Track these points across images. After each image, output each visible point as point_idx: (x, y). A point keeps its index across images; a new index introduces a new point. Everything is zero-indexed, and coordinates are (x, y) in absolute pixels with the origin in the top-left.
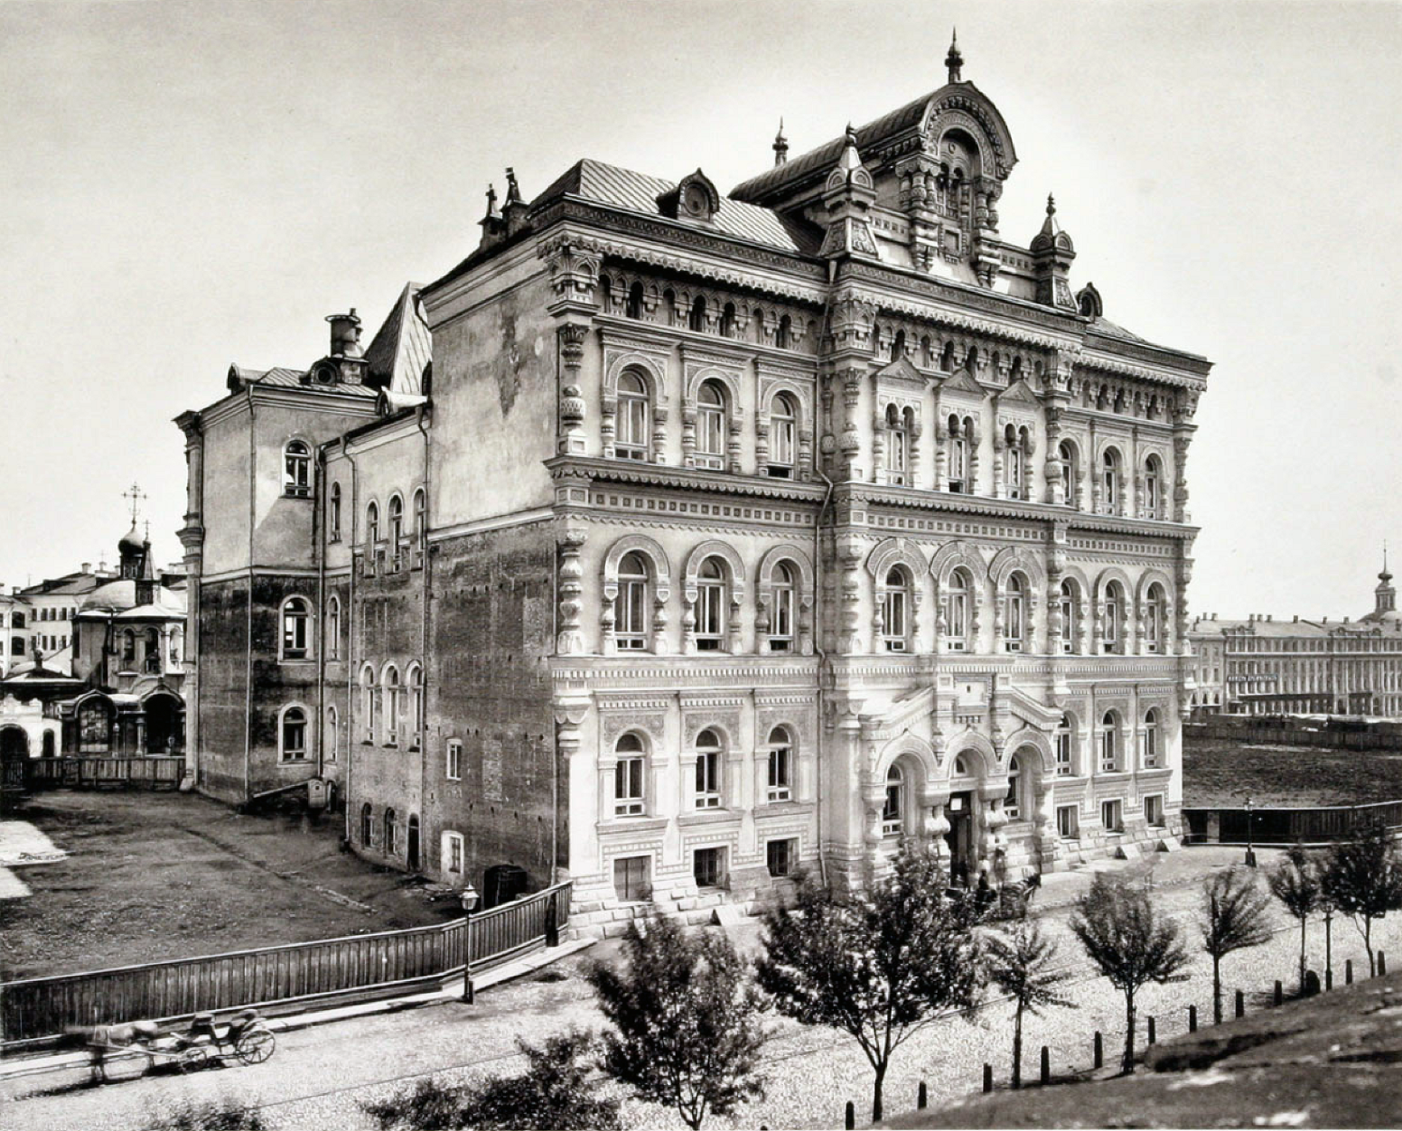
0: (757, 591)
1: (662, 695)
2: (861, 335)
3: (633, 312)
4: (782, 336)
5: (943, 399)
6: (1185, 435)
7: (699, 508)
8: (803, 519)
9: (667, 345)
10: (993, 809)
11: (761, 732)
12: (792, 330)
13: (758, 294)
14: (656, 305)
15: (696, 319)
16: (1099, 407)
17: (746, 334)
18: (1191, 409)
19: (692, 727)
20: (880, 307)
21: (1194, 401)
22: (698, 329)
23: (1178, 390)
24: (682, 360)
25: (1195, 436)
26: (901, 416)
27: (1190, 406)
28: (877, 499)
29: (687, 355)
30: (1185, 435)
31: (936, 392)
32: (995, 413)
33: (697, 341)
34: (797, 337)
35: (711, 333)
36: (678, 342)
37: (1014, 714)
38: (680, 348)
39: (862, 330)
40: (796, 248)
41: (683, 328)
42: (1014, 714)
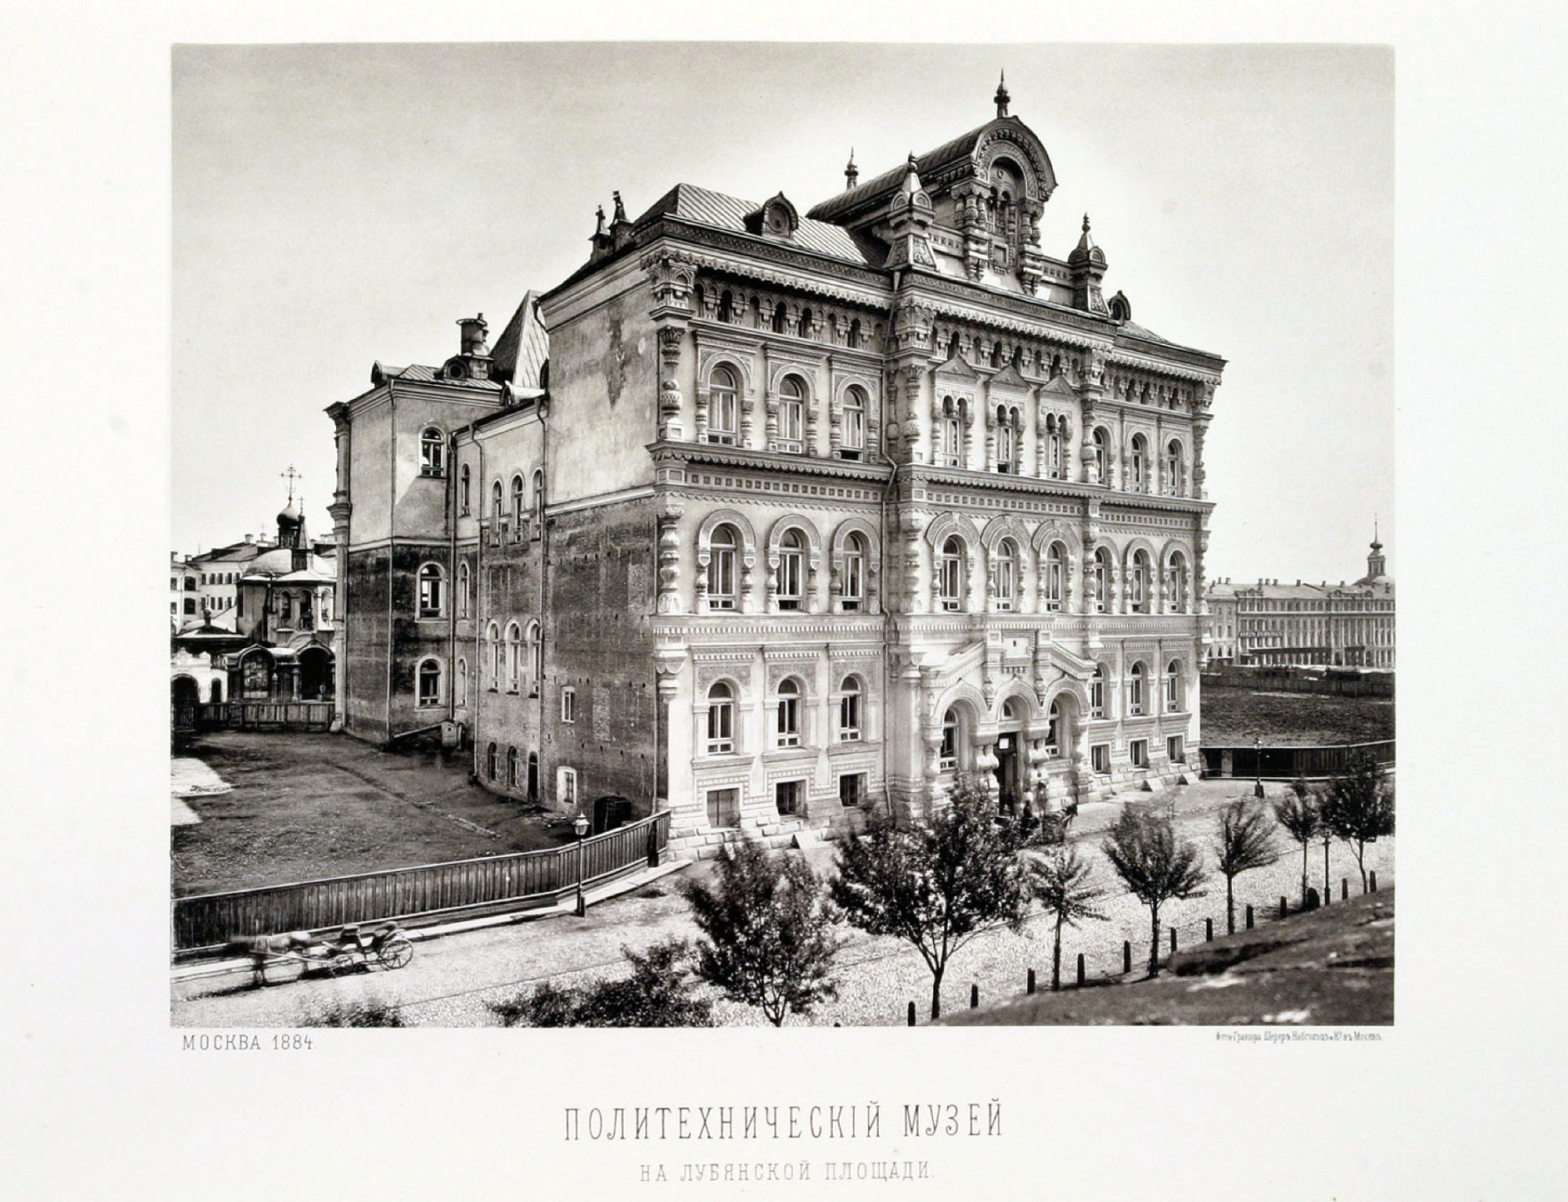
0: (831, 558)
1: (749, 649)
2: (922, 336)
4: (853, 337)
6: (1203, 423)
7: (781, 487)
12: (862, 332)
13: (832, 301)
14: (743, 311)
15: (778, 322)
23: (1196, 384)
25: (1211, 424)
26: (956, 406)
27: (1206, 398)
29: (770, 353)
30: (1203, 423)
34: (865, 338)
35: (791, 335)
37: (1054, 665)
39: (922, 332)
41: (766, 330)
42: (1054, 665)
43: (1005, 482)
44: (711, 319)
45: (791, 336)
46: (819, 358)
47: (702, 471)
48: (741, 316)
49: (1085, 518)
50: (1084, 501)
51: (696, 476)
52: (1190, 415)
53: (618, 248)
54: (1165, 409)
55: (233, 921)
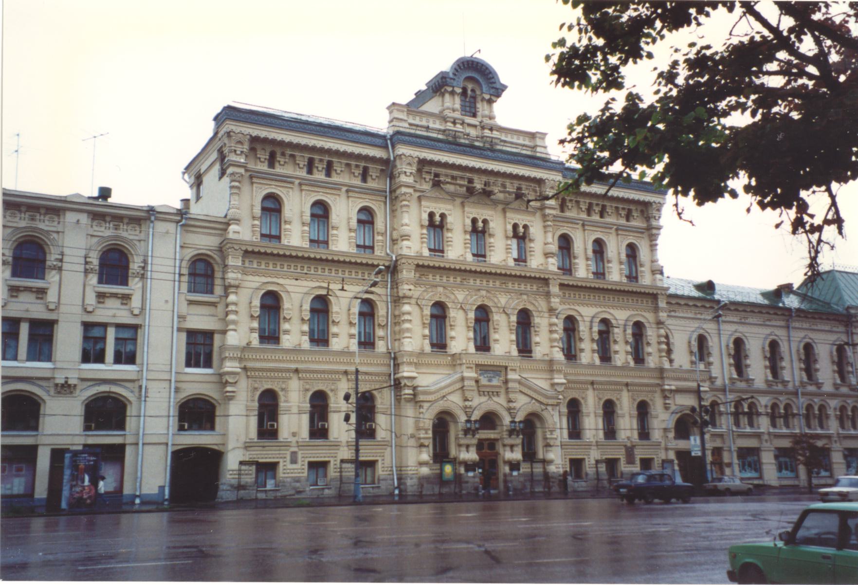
0: (349, 315)
1: (585, 383)
2: (408, 174)
3: (271, 164)
4: (364, 176)
5: (509, 215)
6: (654, 231)
7: (299, 267)
8: (650, 303)
9: (578, 224)
10: (512, 451)
11: (599, 402)
12: (335, 168)
13: (290, 145)
14: (285, 162)
15: (589, 211)
16: (589, 214)
17: (341, 177)
18: (657, 216)
19: (600, 399)
20: (419, 158)
21: (659, 210)
22: (274, 168)
23: (646, 205)
24: (584, 230)
25: (662, 231)
26: (480, 224)
27: (655, 213)
28: (421, 263)
29: (586, 227)
30: (654, 231)
31: (504, 211)
32: (505, 217)
33: (310, 180)
34: (374, 177)
35: (596, 217)
36: (615, 227)
37: (521, 391)
38: (583, 225)
39: (408, 171)
40: (692, 190)
41: (584, 216)
42: (521, 391)
43: (598, 284)
44: (264, 167)
45: (262, 168)
46: (611, 228)
47: (255, 258)
48: (283, 165)
49: (656, 309)
50: (545, 281)
51: (324, 269)
52: (645, 225)
53: (610, 194)
54: (623, 221)
55: (237, 476)
